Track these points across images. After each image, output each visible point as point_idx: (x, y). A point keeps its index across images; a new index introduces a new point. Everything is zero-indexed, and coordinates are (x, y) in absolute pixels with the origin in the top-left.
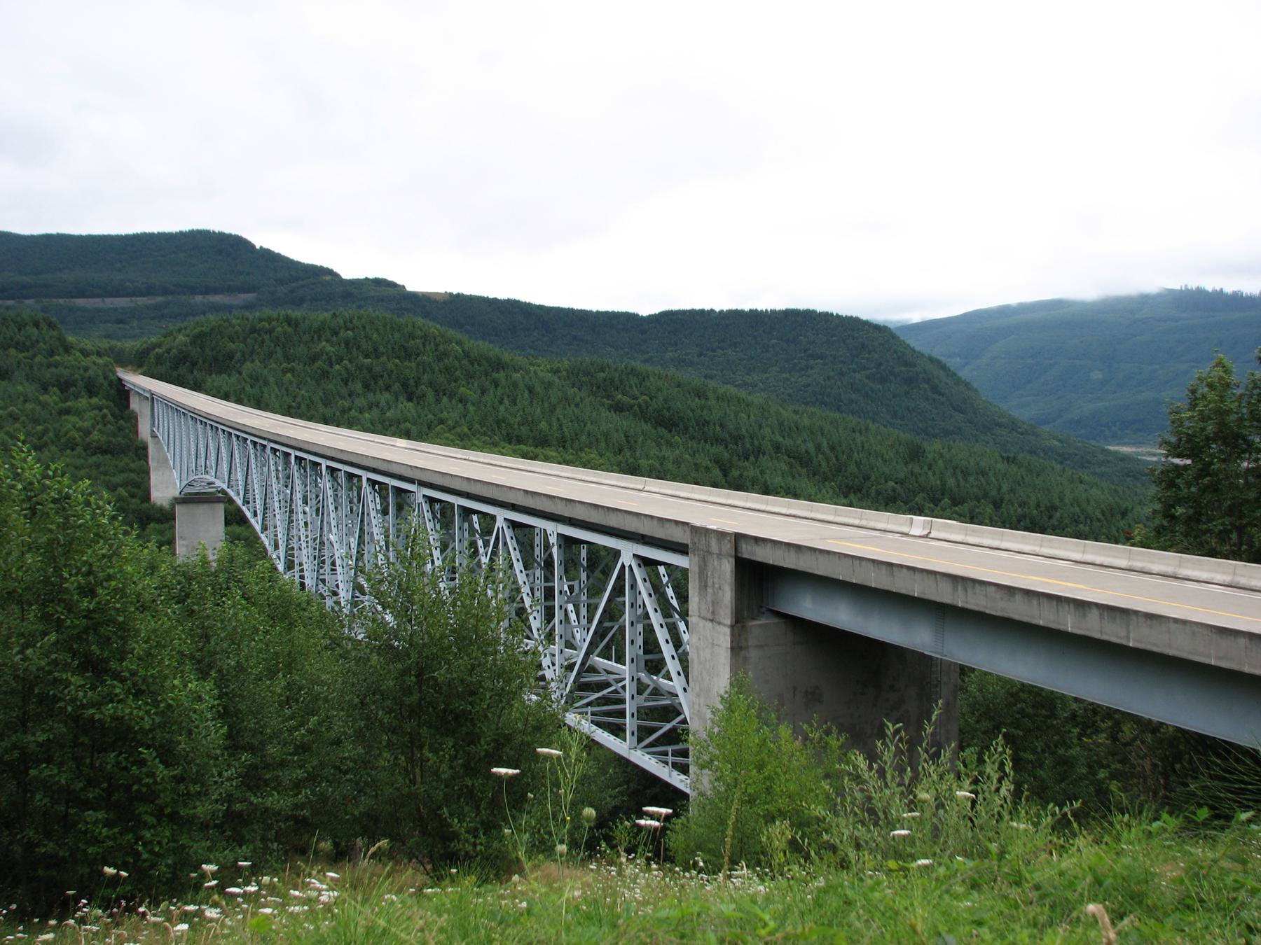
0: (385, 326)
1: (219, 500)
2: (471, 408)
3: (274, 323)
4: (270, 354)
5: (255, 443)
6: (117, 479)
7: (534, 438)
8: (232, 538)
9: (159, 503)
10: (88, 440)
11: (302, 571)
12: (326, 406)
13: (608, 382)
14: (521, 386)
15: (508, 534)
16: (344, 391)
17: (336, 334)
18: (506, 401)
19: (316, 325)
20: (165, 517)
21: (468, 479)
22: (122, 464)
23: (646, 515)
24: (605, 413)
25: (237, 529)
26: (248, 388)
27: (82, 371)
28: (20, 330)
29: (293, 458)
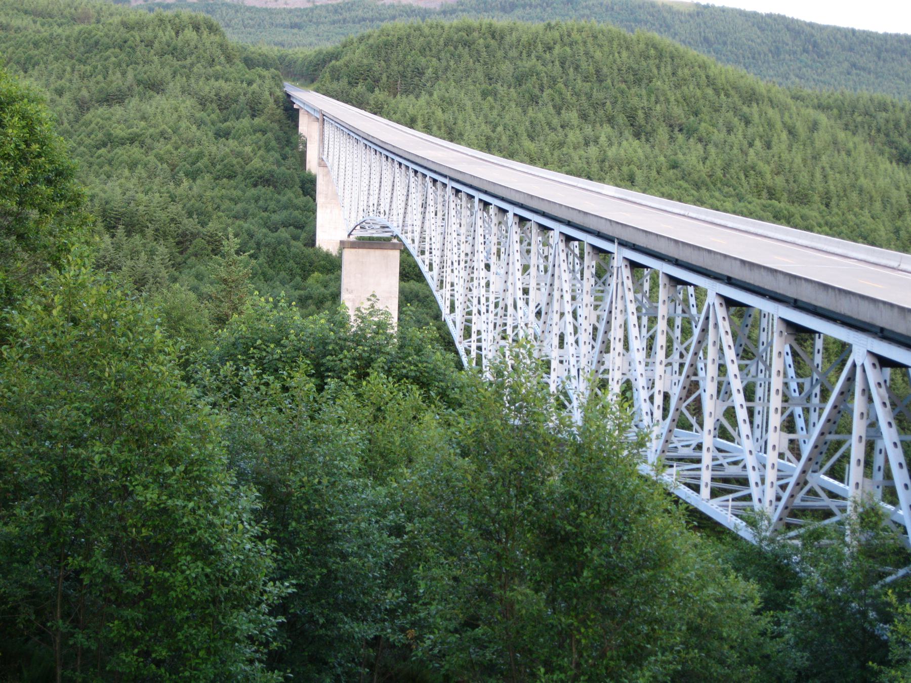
0: (611, 41)
1: (394, 247)
2: (712, 150)
3: (476, 34)
4: (468, 71)
5: (435, 181)
6: (276, 217)
7: (790, 192)
8: (405, 298)
9: (325, 249)
10: (248, 168)
11: (479, 340)
12: (532, 138)
13: (891, 125)
14: (779, 125)
15: (721, 312)
16: (555, 121)
17: (550, 49)
18: (758, 143)
19: (524, 38)
20: (332, 266)
21: (676, 242)
22: (284, 199)
23: (885, 303)
24: (885, 165)
25: (413, 285)
26: (439, 113)
27: (245, 85)
28: (177, 33)
29: (476, 200)
